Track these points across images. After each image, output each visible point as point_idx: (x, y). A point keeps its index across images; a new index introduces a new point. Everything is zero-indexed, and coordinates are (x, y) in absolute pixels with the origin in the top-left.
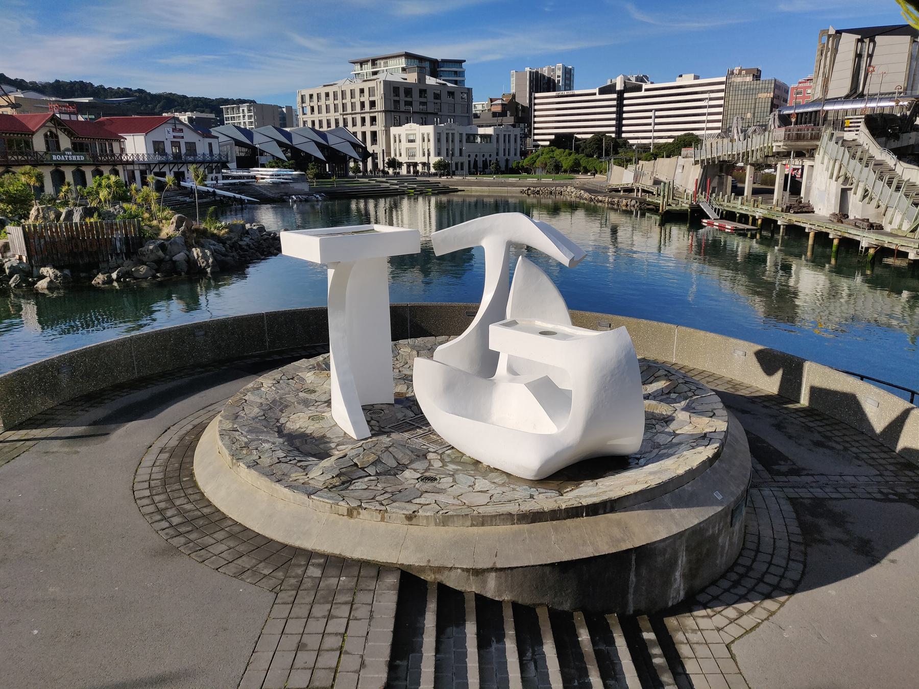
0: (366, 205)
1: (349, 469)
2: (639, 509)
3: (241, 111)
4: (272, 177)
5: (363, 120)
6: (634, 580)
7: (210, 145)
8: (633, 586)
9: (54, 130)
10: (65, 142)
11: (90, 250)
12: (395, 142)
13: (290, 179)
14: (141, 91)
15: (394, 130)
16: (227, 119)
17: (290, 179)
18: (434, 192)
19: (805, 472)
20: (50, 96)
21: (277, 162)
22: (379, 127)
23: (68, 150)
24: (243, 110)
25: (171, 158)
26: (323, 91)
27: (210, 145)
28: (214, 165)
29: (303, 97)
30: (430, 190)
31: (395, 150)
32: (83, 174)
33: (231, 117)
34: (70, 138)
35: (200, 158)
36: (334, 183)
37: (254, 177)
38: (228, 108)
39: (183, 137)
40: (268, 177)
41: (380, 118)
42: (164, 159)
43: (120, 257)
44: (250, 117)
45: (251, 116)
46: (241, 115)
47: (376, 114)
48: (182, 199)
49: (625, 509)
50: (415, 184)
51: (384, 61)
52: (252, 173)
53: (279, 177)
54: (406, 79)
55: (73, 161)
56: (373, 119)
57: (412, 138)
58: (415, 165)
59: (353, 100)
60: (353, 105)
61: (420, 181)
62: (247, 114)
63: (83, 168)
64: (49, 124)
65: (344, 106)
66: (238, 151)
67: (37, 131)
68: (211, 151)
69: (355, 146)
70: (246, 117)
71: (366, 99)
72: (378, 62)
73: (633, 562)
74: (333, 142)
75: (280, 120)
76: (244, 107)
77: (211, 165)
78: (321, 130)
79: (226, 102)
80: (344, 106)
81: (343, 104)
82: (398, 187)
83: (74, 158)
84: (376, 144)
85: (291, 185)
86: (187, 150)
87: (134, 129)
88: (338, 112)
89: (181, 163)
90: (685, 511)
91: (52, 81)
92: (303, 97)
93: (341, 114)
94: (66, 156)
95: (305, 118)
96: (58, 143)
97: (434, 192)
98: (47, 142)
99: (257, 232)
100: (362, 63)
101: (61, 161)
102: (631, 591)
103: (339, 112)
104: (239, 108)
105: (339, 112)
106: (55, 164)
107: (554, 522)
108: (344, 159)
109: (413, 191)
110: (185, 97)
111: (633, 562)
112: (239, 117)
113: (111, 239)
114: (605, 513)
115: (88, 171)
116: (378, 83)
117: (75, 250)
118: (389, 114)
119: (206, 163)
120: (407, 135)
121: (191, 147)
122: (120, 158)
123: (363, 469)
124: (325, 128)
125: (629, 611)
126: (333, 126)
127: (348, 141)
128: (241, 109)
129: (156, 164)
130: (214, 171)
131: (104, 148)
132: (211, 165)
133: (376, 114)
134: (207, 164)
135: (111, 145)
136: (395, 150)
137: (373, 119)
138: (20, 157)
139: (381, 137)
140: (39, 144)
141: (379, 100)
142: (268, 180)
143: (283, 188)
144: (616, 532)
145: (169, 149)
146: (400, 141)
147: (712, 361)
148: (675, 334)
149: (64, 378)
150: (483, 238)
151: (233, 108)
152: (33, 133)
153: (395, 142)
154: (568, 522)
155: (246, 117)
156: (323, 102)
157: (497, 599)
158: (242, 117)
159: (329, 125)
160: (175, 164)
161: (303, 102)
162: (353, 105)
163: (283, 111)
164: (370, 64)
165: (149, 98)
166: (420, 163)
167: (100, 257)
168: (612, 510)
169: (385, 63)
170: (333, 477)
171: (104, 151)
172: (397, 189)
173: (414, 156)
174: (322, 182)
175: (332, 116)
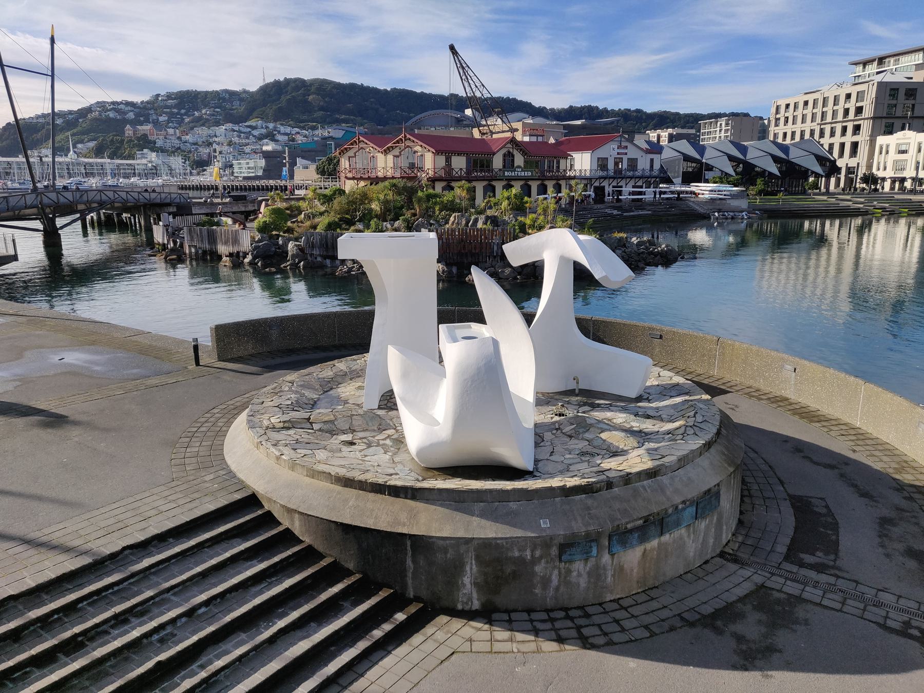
0: (823, 225)
1: (299, 420)
2: (441, 506)
3: (718, 125)
4: (711, 193)
5: (844, 129)
6: (412, 565)
7: (652, 160)
8: (411, 571)
9: (511, 150)
10: (519, 160)
11: (474, 251)
12: (881, 153)
13: (728, 195)
14: (638, 111)
15: (881, 140)
16: (704, 134)
17: (728, 195)
18: (910, 212)
19: (832, 572)
20: (552, 120)
21: (724, 178)
22: (863, 138)
23: (519, 167)
24: (721, 125)
25: (611, 173)
26: (801, 99)
27: (652, 160)
28: (653, 180)
29: (778, 108)
30: (906, 210)
31: (879, 163)
32: (530, 187)
33: (708, 132)
34: (524, 157)
35: (638, 174)
36: (781, 200)
37: (694, 193)
38: (706, 123)
39: (626, 154)
40: (707, 192)
41: (866, 126)
42: (604, 174)
43: (496, 259)
44: (726, 131)
45: (728, 130)
46: (718, 129)
47: (861, 122)
48: (610, 212)
49: (427, 501)
50: (888, 203)
51: (895, 58)
52: (693, 189)
53: (720, 193)
54: (911, 78)
55: (521, 176)
56: (857, 129)
57: (904, 148)
58: (903, 180)
59: (835, 108)
60: (835, 113)
61: (898, 200)
62: (724, 128)
63: (530, 183)
64: (509, 146)
65: (824, 115)
66: (683, 166)
67: (498, 151)
68: (652, 166)
69: (821, 160)
70: (723, 131)
71: (852, 105)
72: (887, 60)
73: (409, 548)
74: (796, 156)
75: (759, 133)
76: (723, 121)
77: (649, 180)
78: (784, 143)
79: (703, 117)
80: (824, 115)
81: (823, 113)
82: (861, 206)
83: (523, 174)
84: (855, 157)
85: (728, 202)
86: (628, 165)
87: (581, 148)
88: (815, 122)
89: (620, 178)
90: (484, 522)
91: (566, 107)
92: (778, 108)
93: (818, 124)
94: (516, 173)
95: (777, 130)
96: (513, 161)
97: (910, 212)
98: (504, 160)
99: (635, 247)
100: (865, 64)
101: (511, 176)
102: (410, 575)
103: (817, 122)
104: (717, 122)
105: (817, 122)
106: (506, 180)
107: (361, 492)
108: (804, 173)
109: (880, 211)
110: (678, 114)
111: (409, 548)
112: (716, 131)
113: (490, 243)
114: (406, 498)
115: (534, 186)
116: (871, 86)
117: (463, 251)
118: (878, 121)
119: (645, 178)
120: (898, 145)
121: (633, 163)
122: (563, 173)
123: (311, 423)
124: (788, 141)
125: (409, 594)
126: (797, 138)
127: (813, 154)
128: (719, 123)
129: (597, 179)
130: (652, 186)
131: (551, 164)
132: (649, 180)
133: (861, 122)
134: (654, 179)
135: (558, 163)
136: (879, 163)
137: (857, 129)
138: (479, 174)
139: (863, 150)
140: (497, 162)
141: (868, 106)
142: (707, 196)
143: (719, 205)
144: (403, 517)
145: (611, 166)
146: (887, 152)
147: (897, 433)
148: (861, 391)
149: (274, 333)
150: (543, 252)
151: (711, 123)
152: (494, 154)
153: (881, 153)
154: (371, 496)
155: (723, 131)
156: (799, 113)
157: (301, 538)
158: (718, 131)
159: (793, 138)
160: (614, 178)
161: (777, 112)
162: (835, 113)
163: (764, 123)
164: (875, 63)
165: (644, 117)
166: (910, 178)
167: (481, 258)
168: (414, 498)
169: (895, 61)
170: (280, 422)
171: (551, 167)
172: (859, 209)
173: (903, 169)
174: (769, 199)
175: (798, 128)
